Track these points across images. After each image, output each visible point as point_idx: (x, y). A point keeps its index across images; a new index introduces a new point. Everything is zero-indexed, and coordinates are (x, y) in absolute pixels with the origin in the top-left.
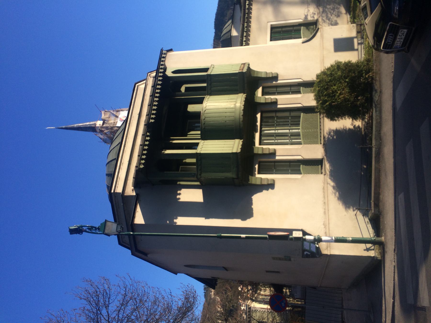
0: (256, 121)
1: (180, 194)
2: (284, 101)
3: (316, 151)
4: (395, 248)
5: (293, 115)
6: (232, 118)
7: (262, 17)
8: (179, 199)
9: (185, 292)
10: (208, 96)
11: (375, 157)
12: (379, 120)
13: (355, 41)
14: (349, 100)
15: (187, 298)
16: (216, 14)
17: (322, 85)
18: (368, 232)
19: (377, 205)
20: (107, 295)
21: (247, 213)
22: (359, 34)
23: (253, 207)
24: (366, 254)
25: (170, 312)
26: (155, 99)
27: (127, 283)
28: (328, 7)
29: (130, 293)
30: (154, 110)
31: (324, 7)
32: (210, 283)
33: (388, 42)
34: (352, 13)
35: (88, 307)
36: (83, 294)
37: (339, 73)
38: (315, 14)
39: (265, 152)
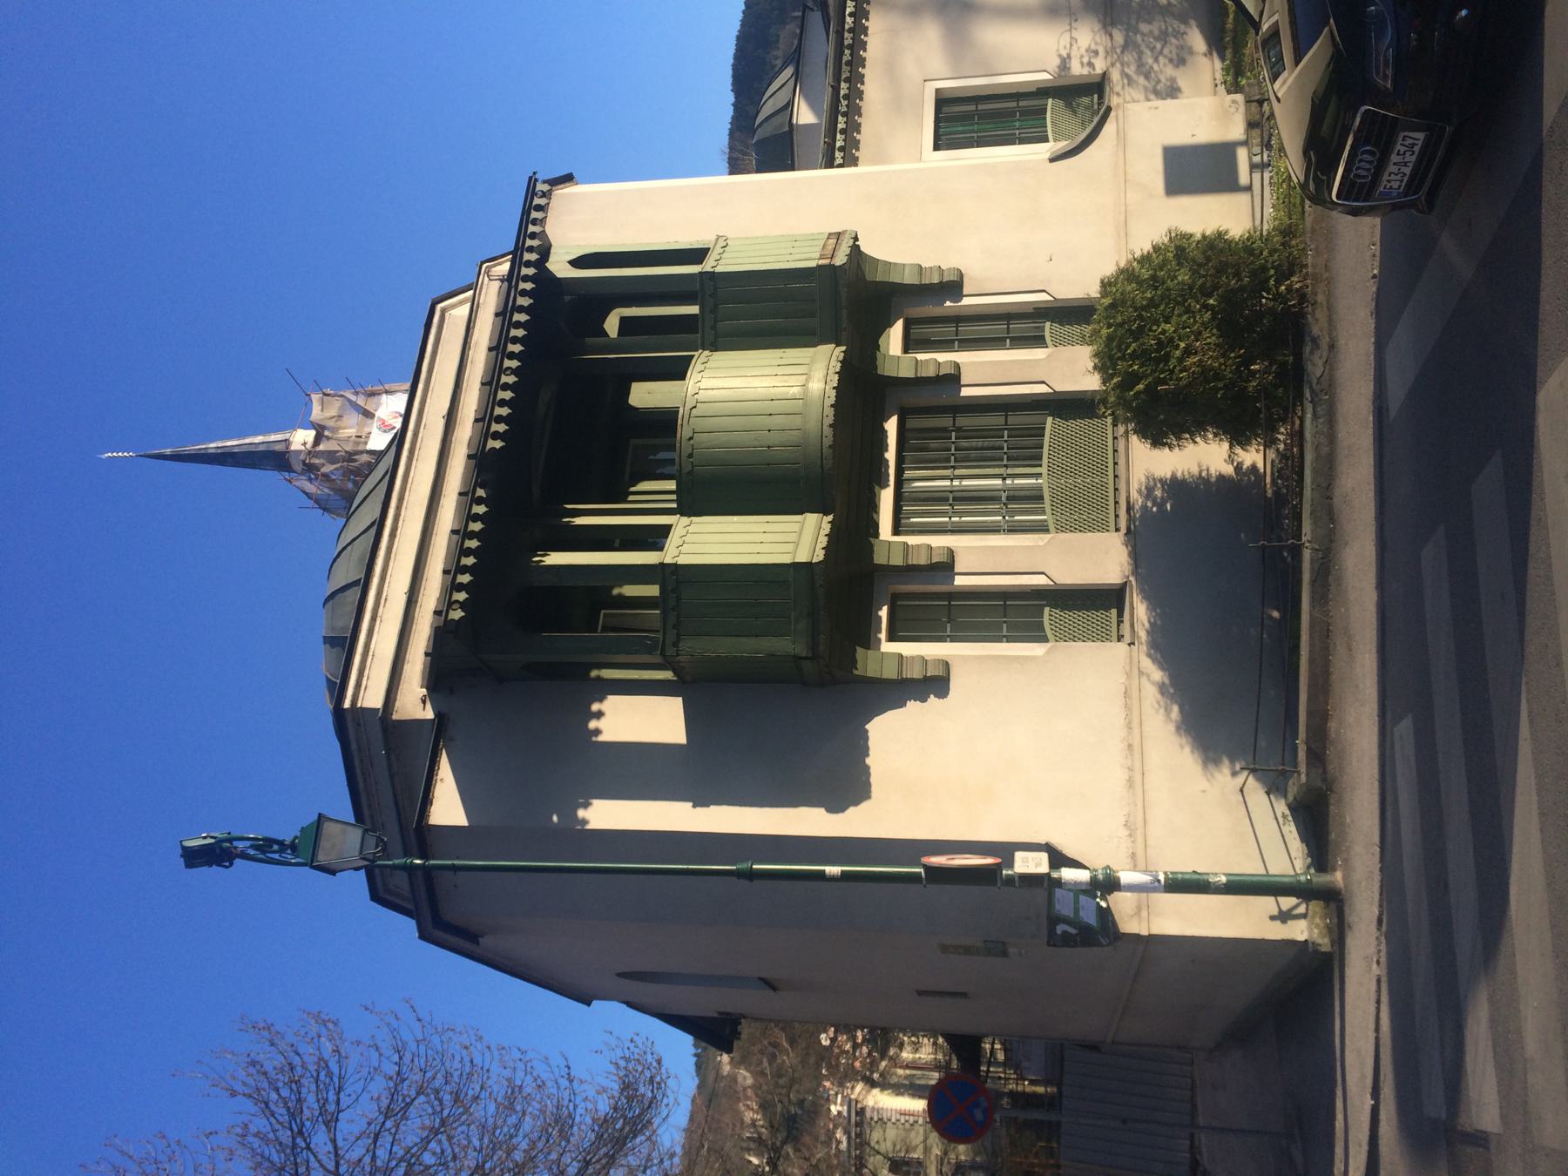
0: (883, 447)
1: (599, 715)
2: (986, 371)
3: (1101, 558)
4: (1381, 914)
5: (1017, 425)
6: (793, 436)
7: (907, 64)
8: (597, 732)
9: (622, 1063)
10: (707, 353)
11: (1313, 582)
12: (1325, 450)
13: (1242, 154)
14: (1217, 376)
15: (627, 1087)
16: (738, 38)
17: (1119, 319)
18: (1285, 855)
19: (1318, 757)
20: (331, 1080)
21: (848, 786)
22: (1256, 132)
23: (868, 761)
24: (1277, 932)
25: (565, 1136)
26: (508, 363)
27: (406, 1035)
28: (1144, 27)
29: (416, 1070)
30: (502, 403)
31: (1130, 30)
32: (714, 1032)
33: (1357, 176)
34: (1229, 54)
35: (260, 1124)
36: (242, 1074)
37: (1184, 276)
38: (1096, 53)
39: (913, 561)
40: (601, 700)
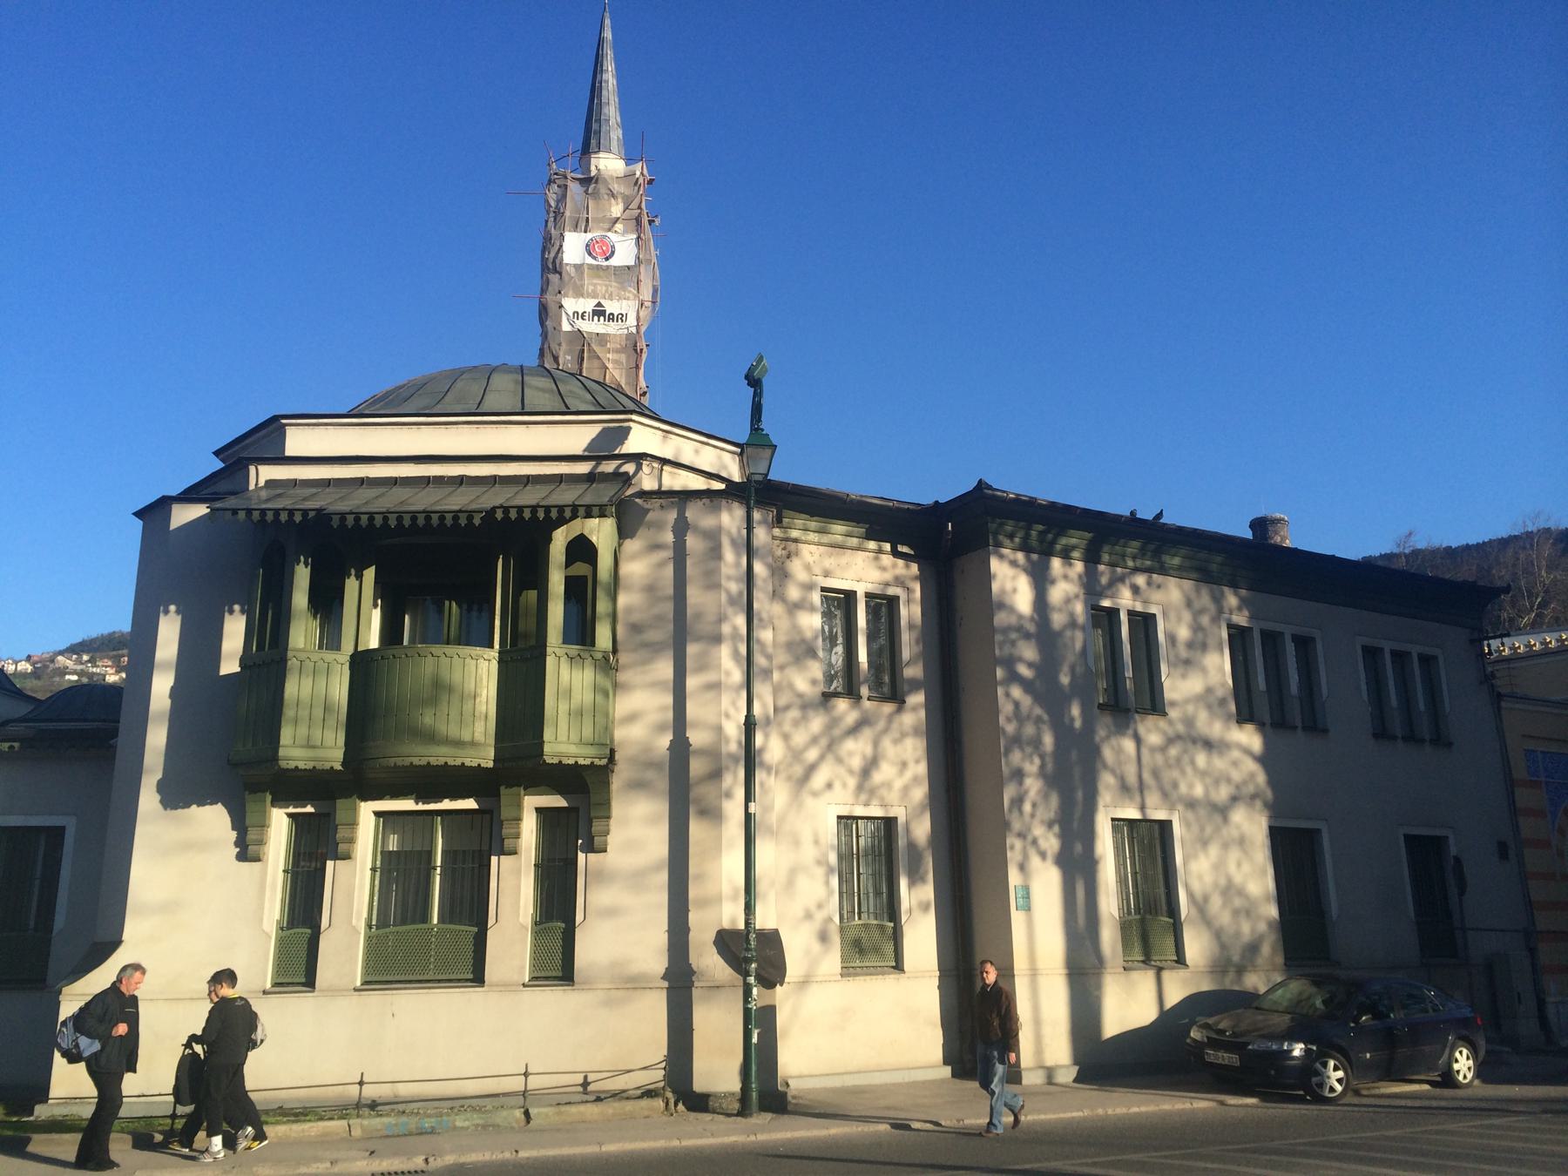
0: (454, 797)
40: (178, 612)
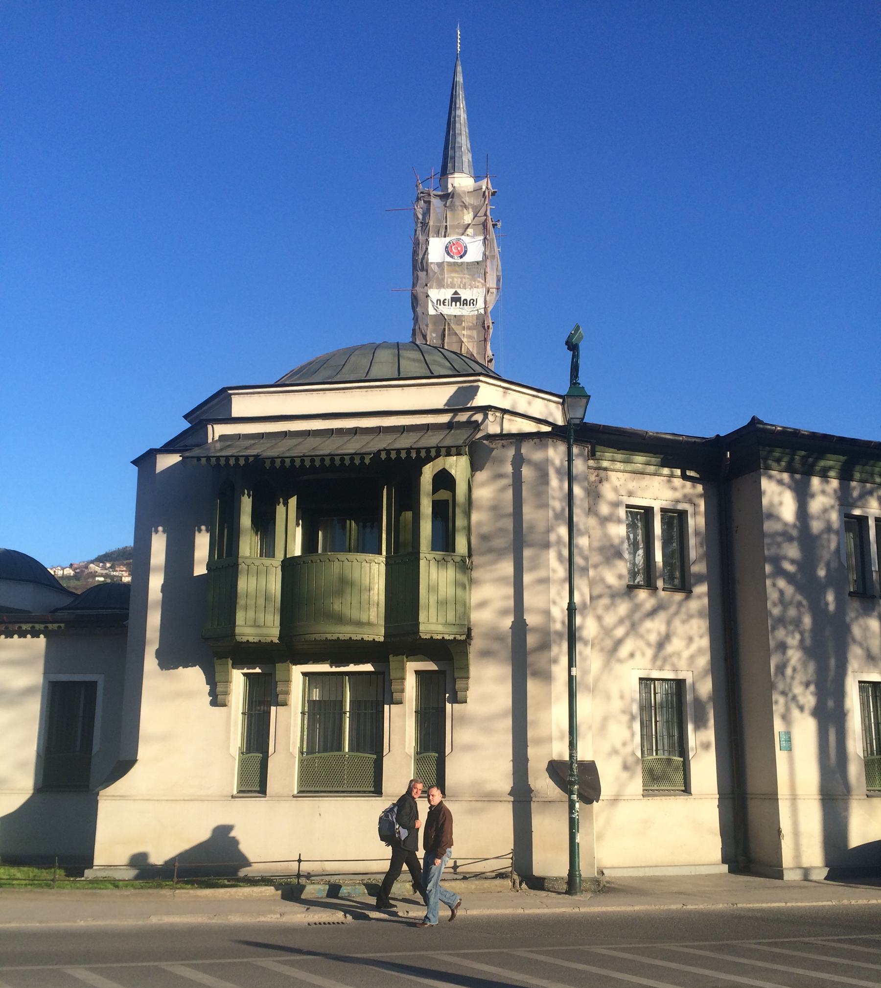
0: (357, 662)
21: (170, 659)
